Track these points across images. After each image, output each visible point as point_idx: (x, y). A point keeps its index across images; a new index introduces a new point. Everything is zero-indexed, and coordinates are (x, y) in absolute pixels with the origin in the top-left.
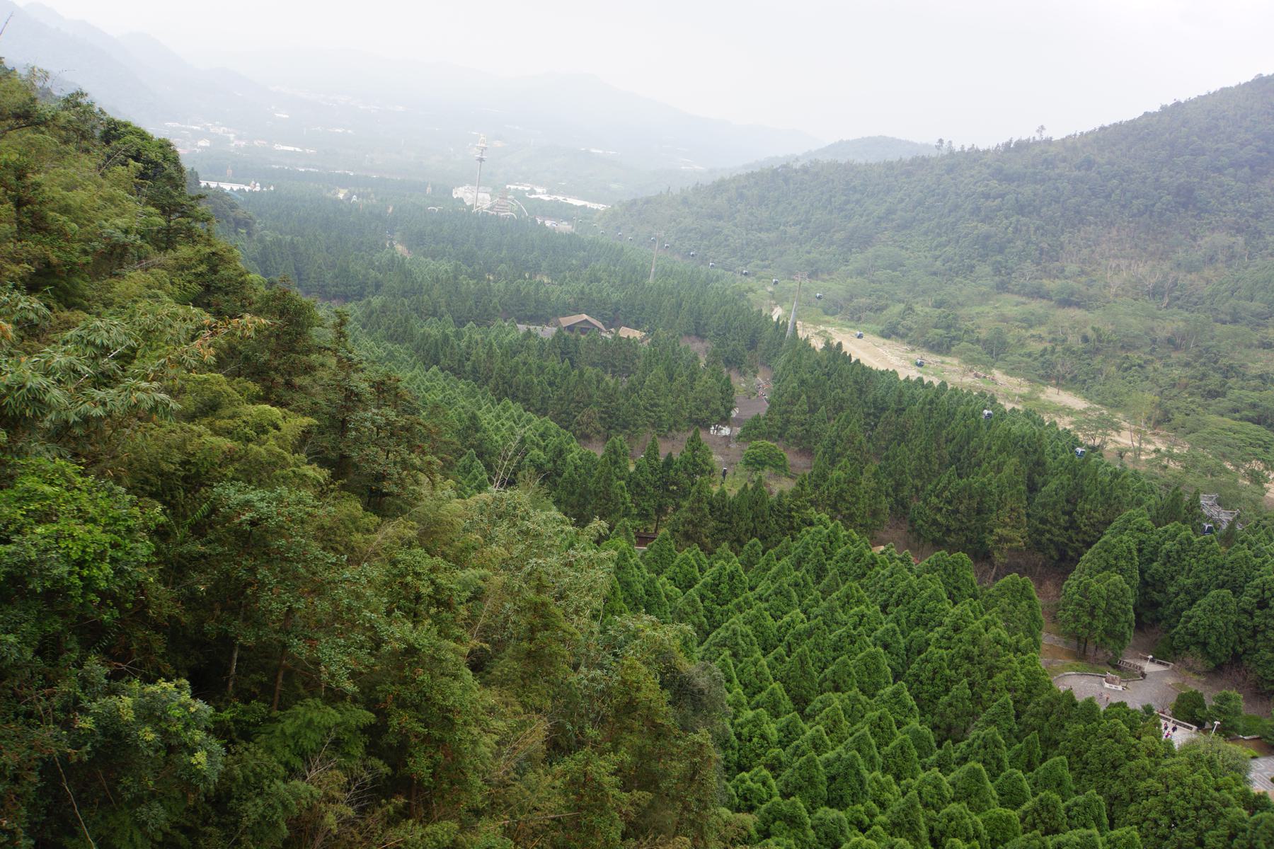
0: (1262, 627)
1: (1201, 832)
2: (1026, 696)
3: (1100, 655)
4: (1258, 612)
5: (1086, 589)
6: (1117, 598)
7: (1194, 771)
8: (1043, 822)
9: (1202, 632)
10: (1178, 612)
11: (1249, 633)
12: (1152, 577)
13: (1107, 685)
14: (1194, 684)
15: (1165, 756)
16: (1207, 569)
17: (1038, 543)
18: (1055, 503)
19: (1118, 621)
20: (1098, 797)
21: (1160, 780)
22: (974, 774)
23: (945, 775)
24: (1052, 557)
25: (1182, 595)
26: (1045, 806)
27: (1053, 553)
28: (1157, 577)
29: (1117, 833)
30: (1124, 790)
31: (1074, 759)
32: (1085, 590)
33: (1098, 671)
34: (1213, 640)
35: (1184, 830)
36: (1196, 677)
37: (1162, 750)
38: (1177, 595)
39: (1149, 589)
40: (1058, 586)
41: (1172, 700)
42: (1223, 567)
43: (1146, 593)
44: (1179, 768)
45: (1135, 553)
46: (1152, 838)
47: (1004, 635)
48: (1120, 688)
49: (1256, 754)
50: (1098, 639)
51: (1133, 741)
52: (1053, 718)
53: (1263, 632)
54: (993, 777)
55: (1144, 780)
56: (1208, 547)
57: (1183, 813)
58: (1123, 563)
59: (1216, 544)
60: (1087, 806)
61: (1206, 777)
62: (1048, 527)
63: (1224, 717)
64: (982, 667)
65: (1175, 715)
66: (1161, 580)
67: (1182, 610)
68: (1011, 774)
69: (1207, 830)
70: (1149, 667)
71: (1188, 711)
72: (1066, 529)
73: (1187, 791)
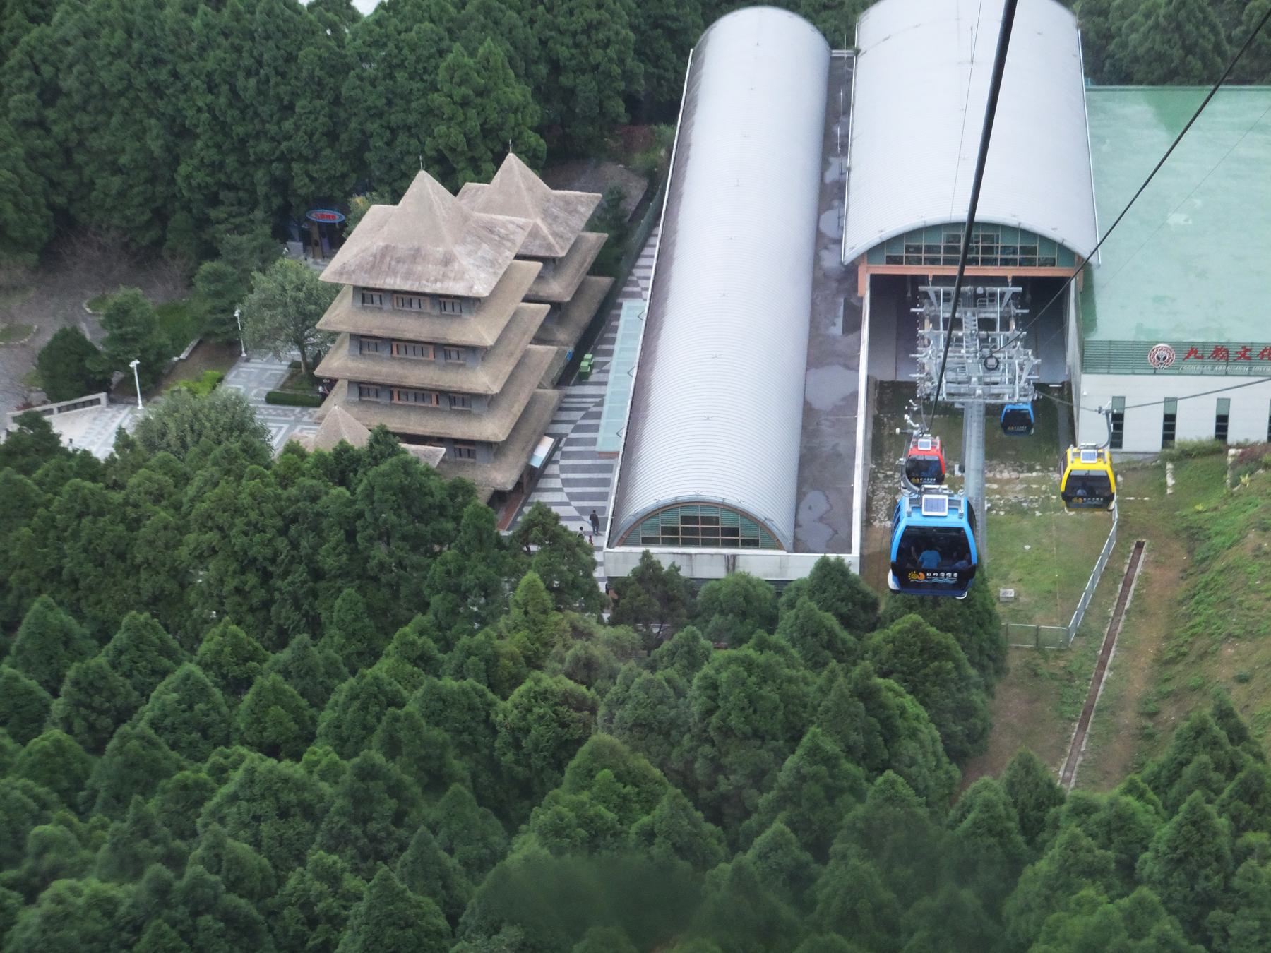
0: (74, 137)
4: (51, 114)
8: (101, 712)
21: (204, 528)
26: (89, 686)
35: (286, 574)
46: (250, 619)
49: (217, 373)
51: (117, 496)
53: (81, 144)
57: (268, 552)
60: (138, 642)
63: (138, 346)
69: (315, 549)
73: (253, 516)
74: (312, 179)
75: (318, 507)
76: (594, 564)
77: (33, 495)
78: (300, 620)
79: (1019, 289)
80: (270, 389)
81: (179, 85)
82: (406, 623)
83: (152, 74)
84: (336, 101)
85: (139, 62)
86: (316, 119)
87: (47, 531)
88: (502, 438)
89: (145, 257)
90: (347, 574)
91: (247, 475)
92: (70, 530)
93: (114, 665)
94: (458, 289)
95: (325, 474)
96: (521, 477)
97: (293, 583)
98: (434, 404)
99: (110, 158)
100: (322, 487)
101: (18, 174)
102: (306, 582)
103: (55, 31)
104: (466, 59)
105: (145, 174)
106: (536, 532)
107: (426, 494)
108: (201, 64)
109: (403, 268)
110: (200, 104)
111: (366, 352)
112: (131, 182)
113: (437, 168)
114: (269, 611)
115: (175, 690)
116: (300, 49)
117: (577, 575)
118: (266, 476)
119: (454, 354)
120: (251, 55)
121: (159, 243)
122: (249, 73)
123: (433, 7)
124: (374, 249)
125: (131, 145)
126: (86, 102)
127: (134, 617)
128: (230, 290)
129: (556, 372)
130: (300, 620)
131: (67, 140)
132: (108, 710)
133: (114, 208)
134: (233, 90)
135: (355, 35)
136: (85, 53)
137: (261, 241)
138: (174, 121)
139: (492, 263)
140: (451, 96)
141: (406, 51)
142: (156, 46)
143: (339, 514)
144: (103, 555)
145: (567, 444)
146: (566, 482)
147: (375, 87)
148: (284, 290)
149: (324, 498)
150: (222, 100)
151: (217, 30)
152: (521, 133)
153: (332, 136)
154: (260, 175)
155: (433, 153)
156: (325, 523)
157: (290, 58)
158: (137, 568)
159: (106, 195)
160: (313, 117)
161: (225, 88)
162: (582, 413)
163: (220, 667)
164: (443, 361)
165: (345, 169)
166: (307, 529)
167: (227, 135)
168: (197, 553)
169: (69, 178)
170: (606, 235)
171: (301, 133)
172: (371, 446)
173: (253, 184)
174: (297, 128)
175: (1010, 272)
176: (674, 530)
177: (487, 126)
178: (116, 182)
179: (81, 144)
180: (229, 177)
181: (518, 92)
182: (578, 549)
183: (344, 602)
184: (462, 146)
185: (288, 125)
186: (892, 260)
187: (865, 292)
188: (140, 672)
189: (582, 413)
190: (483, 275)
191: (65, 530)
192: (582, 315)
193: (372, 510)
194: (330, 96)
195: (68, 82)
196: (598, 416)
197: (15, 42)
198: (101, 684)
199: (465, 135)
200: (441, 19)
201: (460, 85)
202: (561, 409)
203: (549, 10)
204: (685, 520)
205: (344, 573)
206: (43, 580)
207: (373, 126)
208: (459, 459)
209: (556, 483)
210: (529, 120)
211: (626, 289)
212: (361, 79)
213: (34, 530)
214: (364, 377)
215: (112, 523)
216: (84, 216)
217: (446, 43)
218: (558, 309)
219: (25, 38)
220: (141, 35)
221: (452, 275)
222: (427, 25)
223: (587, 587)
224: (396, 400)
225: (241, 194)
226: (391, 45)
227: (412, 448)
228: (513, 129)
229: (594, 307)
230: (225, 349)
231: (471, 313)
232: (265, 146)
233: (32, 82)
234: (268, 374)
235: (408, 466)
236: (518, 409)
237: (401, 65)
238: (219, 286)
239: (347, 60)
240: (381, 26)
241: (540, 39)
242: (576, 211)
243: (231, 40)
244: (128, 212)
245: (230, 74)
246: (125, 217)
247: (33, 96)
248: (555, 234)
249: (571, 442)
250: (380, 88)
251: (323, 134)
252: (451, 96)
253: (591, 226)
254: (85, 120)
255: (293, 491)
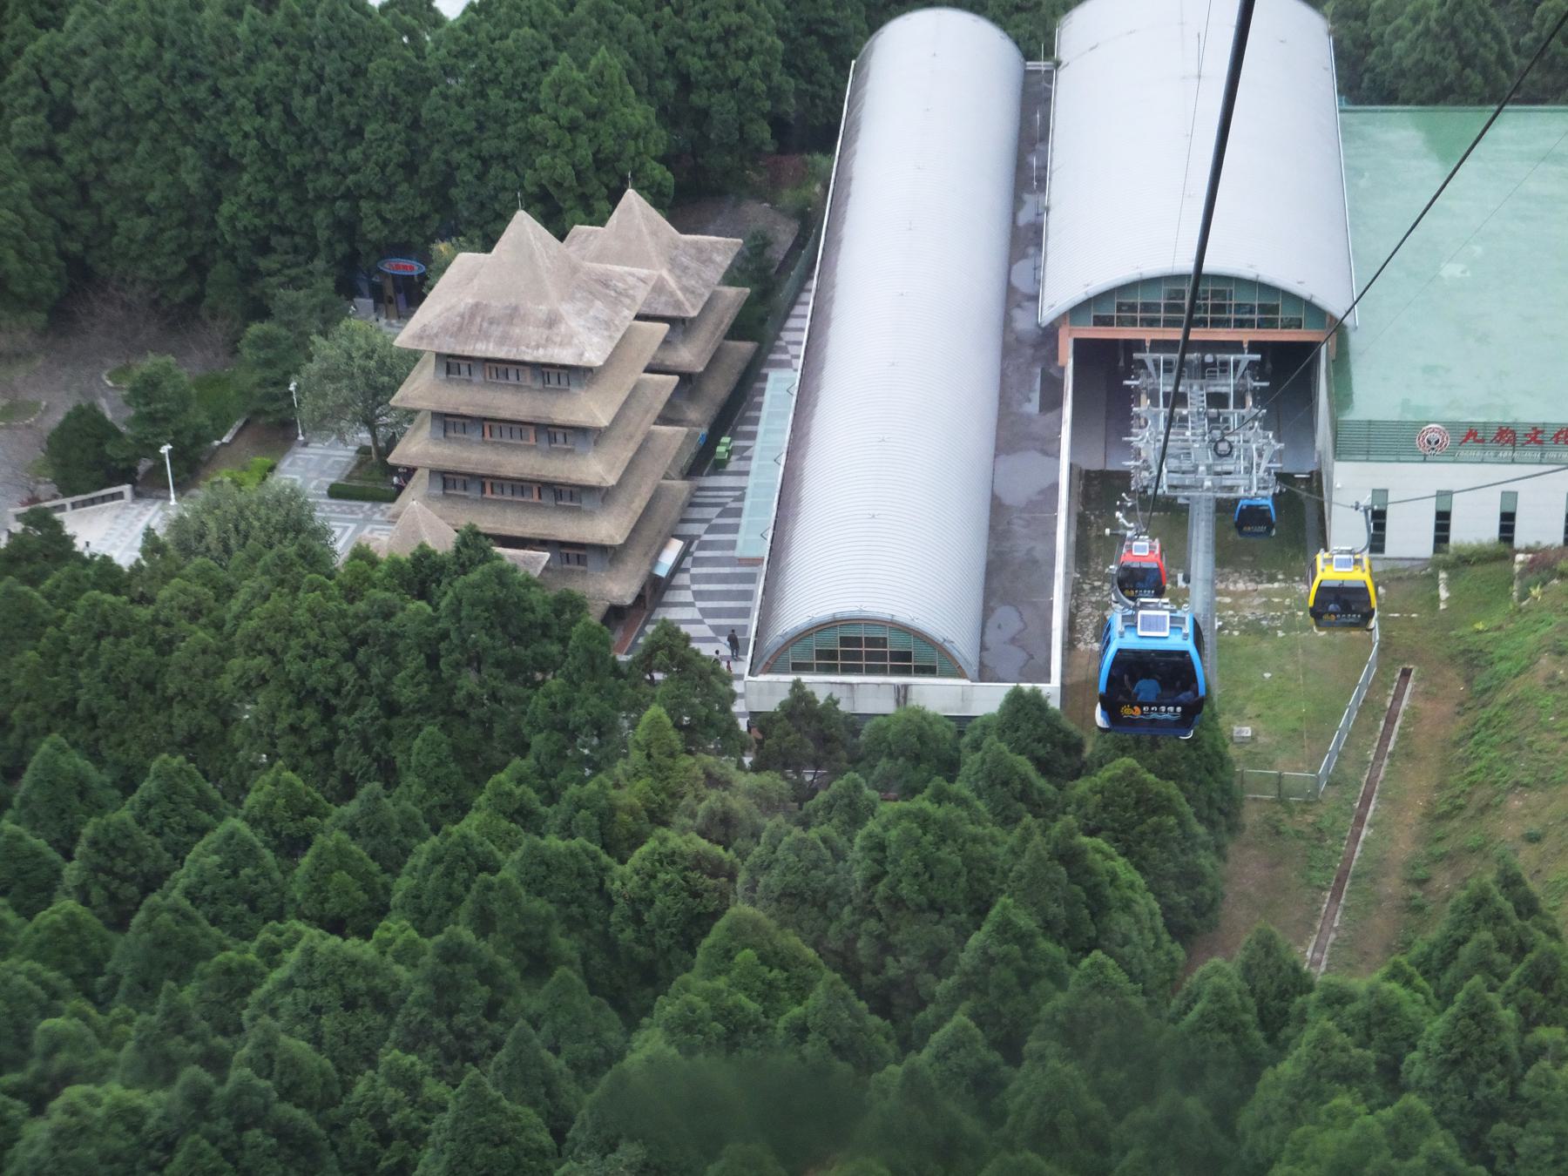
0: (91, 168)
4: (63, 140)
8: (125, 879)
21: (251, 651)
26: (110, 847)
35: (352, 708)
46: (308, 763)
49: (268, 461)
51: (144, 613)
53: (99, 177)
57: (331, 681)
60: (171, 792)
63: (170, 428)
69: (388, 677)
73: (313, 636)
74: (385, 221)
75: (392, 626)
76: (733, 696)
77: (41, 611)
78: (370, 766)
79: (1257, 357)
80: (333, 480)
81: (221, 104)
82: (501, 768)
83: (187, 91)
84: (415, 125)
85: (172, 77)
86: (390, 147)
87: (59, 656)
88: (619, 540)
89: (179, 317)
90: (429, 709)
91: (304, 586)
92: (86, 654)
93: (141, 821)
94: (565, 356)
95: (401, 585)
96: (643, 588)
97: (362, 719)
98: (536, 499)
99: (135, 195)
100: (397, 601)
101: (22, 215)
102: (377, 718)
103: (68, 38)
104: (575, 73)
105: (178, 215)
106: (661, 656)
107: (525, 610)
108: (248, 79)
109: (497, 331)
110: (247, 128)
111: (451, 434)
112: (161, 225)
113: (539, 207)
114: (332, 754)
115: (216, 852)
116: (370, 60)
117: (711, 710)
118: (328, 588)
119: (560, 437)
120: (310, 68)
121: (196, 300)
122: (307, 91)
123: (534, 8)
124: (461, 308)
125: (162, 179)
126: (106, 126)
127: (165, 762)
128: (284, 358)
129: (686, 459)
130: (370, 766)
131: (82, 173)
132: (133, 877)
133: (141, 256)
134: (288, 112)
135: (438, 44)
136: (105, 65)
137: (322, 297)
138: (215, 149)
139: (607, 325)
140: (556, 119)
141: (501, 63)
142: (193, 57)
143: (418, 634)
144: (127, 685)
145: (700, 548)
146: (698, 595)
147: (462, 107)
148: (350, 357)
149: (400, 615)
150: (274, 124)
151: (268, 37)
152: (642, 164)
153: (410, 168)
154: (321, 216)
155: (535, 189)
156: (401, 646)
157: (358, 72)
158: (169, 701)
159: (131, 241)
160: (386, 144)
161: (277, 109)
162: (718, 510)
163: (272, 823)
164: (546, 445)
165: (426, 208)
166: (378, 653)
167: (280, 167)
168: (243, 683)
169: (85, 220)
170: (748, 290)
171: (371, 164)
172: (458, 550)
173: (312, 227)
174: (367, 158)
175: (1246, 336)
176: (832, 655)
177: (601, 156)
178: (144, 225)
179: (99, 177)
180: (283, 219)
181: (639, 114)
182: (712, 678)
183: (425, 742)
184: (570, 180)
185: (355, 154)
186: (1100, 321)
187: (1067, 361)
188: (173, 829)
189: (718, 510)
190: (596, 340)
191: (80, 654)
192: (718, 389)
193: (459, 629)
194: (407, 118)
195: (84, 102)
196: (738, 513)
197: (18, 52)
198: (125, 844)
199: (574, 166)
200: (544, 23)
201: (567, 105)
202: (692, 505)
203: (677, 12)
204: (845, 641)
205: (424, 708)
206: (54, 715)
207: (460, 156)
208: (566, 566)
209: (686, 596)
210: (652, 148)
211: (773, 357)
212: (445, 97)
213: (42, 654)
214: (449, 465)
215: (138, 645)
216: (104, 266)
217: (550, 53)
218: (688, 381)
219: (31, 47)
220: (173, 43)
221: (558, 339)
222: (527, 31)
223: (724, 724)
224: (488, 494)
225: (298, 239)
226: (482, 56)
227: (508, 553)
228: (633, 159)
229: (733, 378)
230: (278, 430)
231: (581, 386)
232: (327, 180)
233: (39, 101)
234: (330, 461)
235: (503, 576)
236: (639, 504)
237: (495, 81)
238: (270, 353)
239: (429, 74)
240: (470, 32)
241: (666, 48)
242: (711, 260)
243: (285, 49)
244: (158, 262)
245: (283, 91)
246: (155, 268)
247: (40, 118)
248: (685, 289)
249: (704, 546)
250: (469, 109)
251: (399, 165)
252: (556, 119)
253: (729, 279)
254: (105, 148)
255: (361, 606)
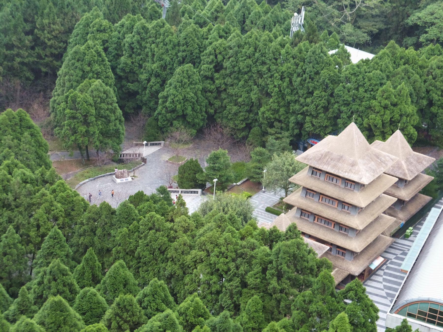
0: (223, 86)
1: (243, 276)
2: (67, 220)
3: (103, 155)
4: (217, 75)
5: (74, 101)
6: (103, 101)
7: (223, 231)
8: (126, 321)
9: (179, 107)
10: (155, 95)
11: (215, 94)
12: (123, 70)
13: (118, 181)
14: (188, 154)
15: (197, 227)
16: (167, 50)
17: (10, 69)
18: (15, 27)
19: (109, 121)
20: (159, 283)
21: (200, 249)
22: (58, 307)
23: (32, 318)
24: (28, 79)
25: (153, 80)
26: (123, 308)
27: (28, 74)
28: (127, 70)
29: (183, 305)
30: (176, 267)
31: (129, 258)
32: (74, 103)
33: (106, 171)
34: (189, 111)
35: (230, 280)
36: (186, 146)
37: (193, 224)
38: (149, 80)
39: (124, 82)
40: (44, 105)
41: (175, 173)
42: (179, 44)
43: (122, 87)
44: (211, 233)
45: (103, 54)
46: (209, 297)
47: (28, 172)
48: (130, 179)
49: (249, 194)
50: (98, 143)
51: (169, 225)
52: (99, 232)
53: (225, 90)
54: (71, 301)
55: (189, 253)
56: (162, 31)
57: (225, 268)
58: (96, 67)
59: (167, 25)
60: (154, 294)
61: (232, 232)
62: (15, 51)
63: (219, 174)
64: (22, 209)
65: (181, 185)
66: (132, 71)
67: (157, 92)
68: (85, 293)
69: (246, 273)
70: (146, 151)
71: (191, 179)
72: (33, 48)
73: (223, 249)
74: (313, 125)
75: (253, 253)
76: (377, 318)
77: (134, 215)
78: (230, 305)
80: (269, 206)
81: (269, 74)
82: (278, 320)
83: (260, 68)
84: (332, 95)
85: (256, 62)
86: (321, 100)
87: (135, 232)
88: (359, 251)
89: (237, 142)
90: (258, 288)
91: (227, 229)
92: (144, 234)
93: (140, 302)
94: (355, 178)
95: (262, 239)
96: (364, 271)
97: (232, 285)
98: (332, 228)
99: (234, 98)
100: (258, 245)
101: (197, 96)
102: (238, 287)
103: (228, 42)
104: (391, 89)
105: (247, 108)
106: (351, 293)
107: (305, 261)
108: (281, 68)
109: (333, 163)
110: (276, 84)
111: (308, 196)
112: (240, 110)
113: (367, 132)
114: (218, 296)
115: (160, 321)
116: (322, 70)
117: (366, 321)
118: (235, 233)
119: (346, 207)
120: (302, 68)
121: (245, 138)
122: (299, 75)
123: (383, 65)
124: (322, 152)
125: (244, 95)
126: (231, 73)
127: (156, 281)
128: (263, 160)
129: (393, 230)
130: (230, 305)
131: (220, 87)
132: (129, 321)
133: (231, 119)
134: (291, 82)
135: (347, 69)
136: (236, 53)
137: (284, 144)
138: (264, 89)
139: (374, 171)
140: (380, 103)
141: (366, 80)
142: (265, 57)
143: (261, 259)
144: (155, 249)
145: (390, 263)
146: (385, 280)
147: (349, 92)
148: (284, 164)
149: (257, 250)
150: (285, 84)
151: (291, 55)
152: (407, 126)
153: (326, 109)
154: (292, 119)
155: (367, 126)
156: (254, 261)
157: (317, 73)
158: (167, 259)
159: (230, 113)
160: (320, 99)
161: (287, 80)
162: (401, 252)
163: (186, 316)
164: (341, 209)
165: (328, 124)
166: (245, 262)
167: (283, 99)
168: (194, 260)
169: (217, 103)
170: (433, 178)
171: (313, 105)
172: (287, 232)
173: (289, 122)
174: (312, 102)
176: (425, 314)
177: (393, 119)
178: (235, 109)
179: (225, 90)
180: (280, 117)
181: (411, 109)
182: (370, 308)
183: (252, 302)
184: (380, 125)
185: (309, 100)
188: (151, 308)
189: (401, 252)
190: (368, 175)
191: (142, 234)
192: (413, 209)
193: (277, 261)
194: (329, 92)
195: (226, 64)
196: (405, 254)
197: (211, 43)
198: (129, 308)
199: (382, 121)
200: (385, 71)
201: (386, 99)
202: (391, 247)
203: (434, 79)
204: (431, 310)
205: (256, 288)
206: (127, 254)
207: (343, 108)
208: (337, 255)
209: (380, 279)
210: (412, 122)
211: (437, 205)
212: (344, 88)
213: (129, 230)
214: (304, 207)
215: (163, 236)
216: (219, 120)
217: (384, 81)
218: (400, 202)
219: (215, 43)
220: (260, 51)
221: (354, 171)
222: (378, 72)
223: (371, 328)
224: (316, 222)
225: (283, 125)
226: (361, 76)
227: (307, 240)
228: (404, 123)
229: (420, 207)
230: (256, 185)
231: (358, 190)
232: (297, 107)
233: (213, 61)
234: (270, 199)
235: (299, 246)
236: (370, 240)
237: (363, 86)
238: (260, 158)
239: (341, 79)
240: (359, 68)
241: (427, 90)
242: (422, 163)
243: (295, 60)
244: (236, 122)
245: (291, 74)
246: (234, 124)
247: (211, 66)
248: (409, 170)
249: (392, 263)
250: (351, 93)
251: (322, 107)
252: (380, 103)
253: (426, 171)
254: (229, 80)
255: (244, 243)
